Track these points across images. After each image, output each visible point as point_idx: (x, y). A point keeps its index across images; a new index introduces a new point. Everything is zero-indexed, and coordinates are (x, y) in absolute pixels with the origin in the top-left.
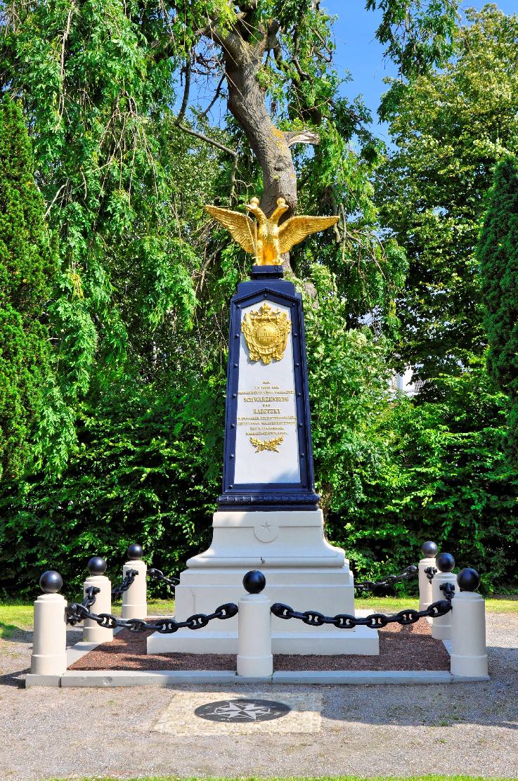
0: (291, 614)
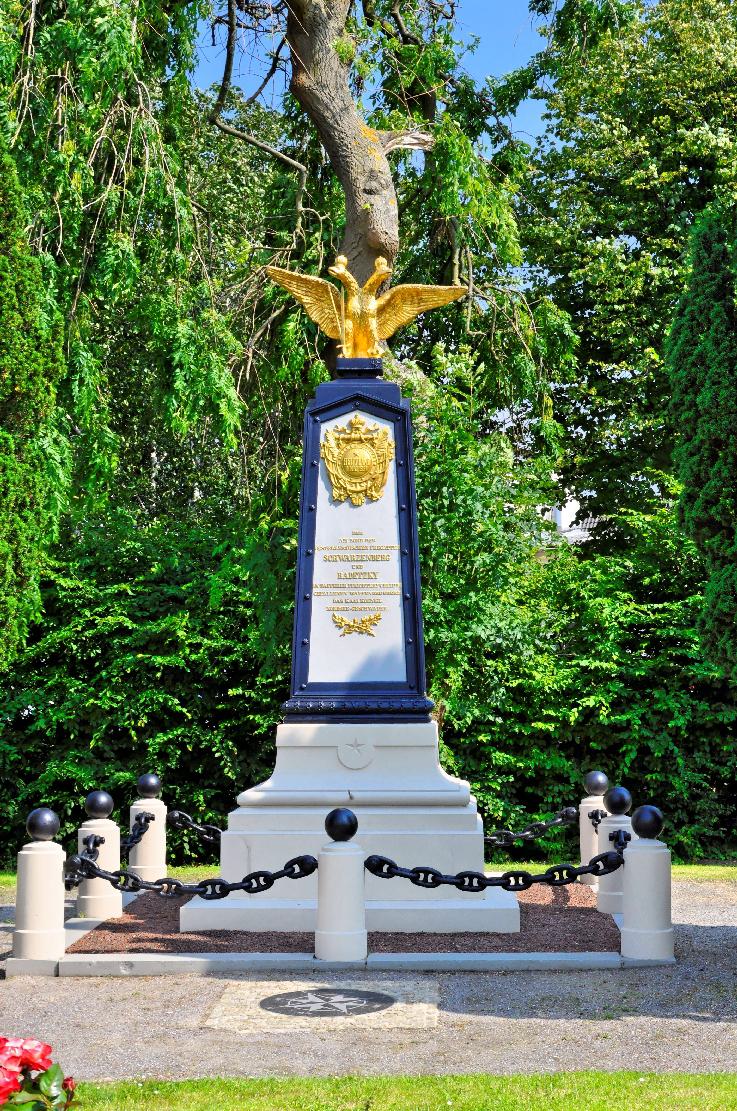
0: (394, 871)
